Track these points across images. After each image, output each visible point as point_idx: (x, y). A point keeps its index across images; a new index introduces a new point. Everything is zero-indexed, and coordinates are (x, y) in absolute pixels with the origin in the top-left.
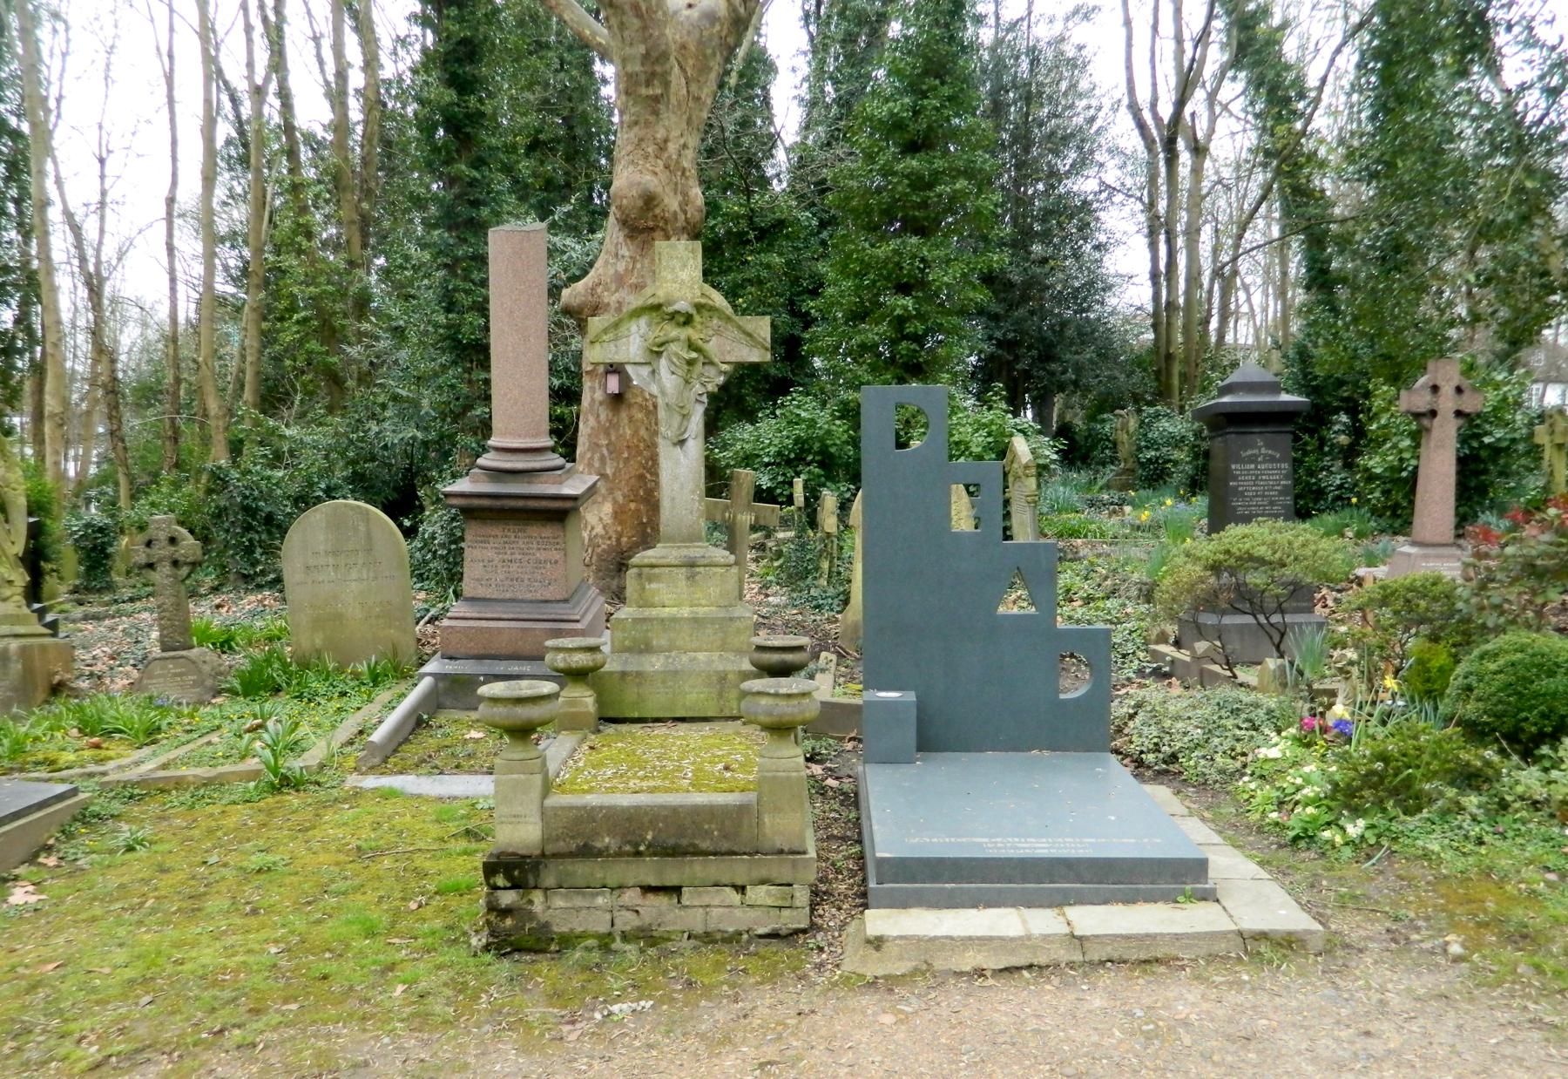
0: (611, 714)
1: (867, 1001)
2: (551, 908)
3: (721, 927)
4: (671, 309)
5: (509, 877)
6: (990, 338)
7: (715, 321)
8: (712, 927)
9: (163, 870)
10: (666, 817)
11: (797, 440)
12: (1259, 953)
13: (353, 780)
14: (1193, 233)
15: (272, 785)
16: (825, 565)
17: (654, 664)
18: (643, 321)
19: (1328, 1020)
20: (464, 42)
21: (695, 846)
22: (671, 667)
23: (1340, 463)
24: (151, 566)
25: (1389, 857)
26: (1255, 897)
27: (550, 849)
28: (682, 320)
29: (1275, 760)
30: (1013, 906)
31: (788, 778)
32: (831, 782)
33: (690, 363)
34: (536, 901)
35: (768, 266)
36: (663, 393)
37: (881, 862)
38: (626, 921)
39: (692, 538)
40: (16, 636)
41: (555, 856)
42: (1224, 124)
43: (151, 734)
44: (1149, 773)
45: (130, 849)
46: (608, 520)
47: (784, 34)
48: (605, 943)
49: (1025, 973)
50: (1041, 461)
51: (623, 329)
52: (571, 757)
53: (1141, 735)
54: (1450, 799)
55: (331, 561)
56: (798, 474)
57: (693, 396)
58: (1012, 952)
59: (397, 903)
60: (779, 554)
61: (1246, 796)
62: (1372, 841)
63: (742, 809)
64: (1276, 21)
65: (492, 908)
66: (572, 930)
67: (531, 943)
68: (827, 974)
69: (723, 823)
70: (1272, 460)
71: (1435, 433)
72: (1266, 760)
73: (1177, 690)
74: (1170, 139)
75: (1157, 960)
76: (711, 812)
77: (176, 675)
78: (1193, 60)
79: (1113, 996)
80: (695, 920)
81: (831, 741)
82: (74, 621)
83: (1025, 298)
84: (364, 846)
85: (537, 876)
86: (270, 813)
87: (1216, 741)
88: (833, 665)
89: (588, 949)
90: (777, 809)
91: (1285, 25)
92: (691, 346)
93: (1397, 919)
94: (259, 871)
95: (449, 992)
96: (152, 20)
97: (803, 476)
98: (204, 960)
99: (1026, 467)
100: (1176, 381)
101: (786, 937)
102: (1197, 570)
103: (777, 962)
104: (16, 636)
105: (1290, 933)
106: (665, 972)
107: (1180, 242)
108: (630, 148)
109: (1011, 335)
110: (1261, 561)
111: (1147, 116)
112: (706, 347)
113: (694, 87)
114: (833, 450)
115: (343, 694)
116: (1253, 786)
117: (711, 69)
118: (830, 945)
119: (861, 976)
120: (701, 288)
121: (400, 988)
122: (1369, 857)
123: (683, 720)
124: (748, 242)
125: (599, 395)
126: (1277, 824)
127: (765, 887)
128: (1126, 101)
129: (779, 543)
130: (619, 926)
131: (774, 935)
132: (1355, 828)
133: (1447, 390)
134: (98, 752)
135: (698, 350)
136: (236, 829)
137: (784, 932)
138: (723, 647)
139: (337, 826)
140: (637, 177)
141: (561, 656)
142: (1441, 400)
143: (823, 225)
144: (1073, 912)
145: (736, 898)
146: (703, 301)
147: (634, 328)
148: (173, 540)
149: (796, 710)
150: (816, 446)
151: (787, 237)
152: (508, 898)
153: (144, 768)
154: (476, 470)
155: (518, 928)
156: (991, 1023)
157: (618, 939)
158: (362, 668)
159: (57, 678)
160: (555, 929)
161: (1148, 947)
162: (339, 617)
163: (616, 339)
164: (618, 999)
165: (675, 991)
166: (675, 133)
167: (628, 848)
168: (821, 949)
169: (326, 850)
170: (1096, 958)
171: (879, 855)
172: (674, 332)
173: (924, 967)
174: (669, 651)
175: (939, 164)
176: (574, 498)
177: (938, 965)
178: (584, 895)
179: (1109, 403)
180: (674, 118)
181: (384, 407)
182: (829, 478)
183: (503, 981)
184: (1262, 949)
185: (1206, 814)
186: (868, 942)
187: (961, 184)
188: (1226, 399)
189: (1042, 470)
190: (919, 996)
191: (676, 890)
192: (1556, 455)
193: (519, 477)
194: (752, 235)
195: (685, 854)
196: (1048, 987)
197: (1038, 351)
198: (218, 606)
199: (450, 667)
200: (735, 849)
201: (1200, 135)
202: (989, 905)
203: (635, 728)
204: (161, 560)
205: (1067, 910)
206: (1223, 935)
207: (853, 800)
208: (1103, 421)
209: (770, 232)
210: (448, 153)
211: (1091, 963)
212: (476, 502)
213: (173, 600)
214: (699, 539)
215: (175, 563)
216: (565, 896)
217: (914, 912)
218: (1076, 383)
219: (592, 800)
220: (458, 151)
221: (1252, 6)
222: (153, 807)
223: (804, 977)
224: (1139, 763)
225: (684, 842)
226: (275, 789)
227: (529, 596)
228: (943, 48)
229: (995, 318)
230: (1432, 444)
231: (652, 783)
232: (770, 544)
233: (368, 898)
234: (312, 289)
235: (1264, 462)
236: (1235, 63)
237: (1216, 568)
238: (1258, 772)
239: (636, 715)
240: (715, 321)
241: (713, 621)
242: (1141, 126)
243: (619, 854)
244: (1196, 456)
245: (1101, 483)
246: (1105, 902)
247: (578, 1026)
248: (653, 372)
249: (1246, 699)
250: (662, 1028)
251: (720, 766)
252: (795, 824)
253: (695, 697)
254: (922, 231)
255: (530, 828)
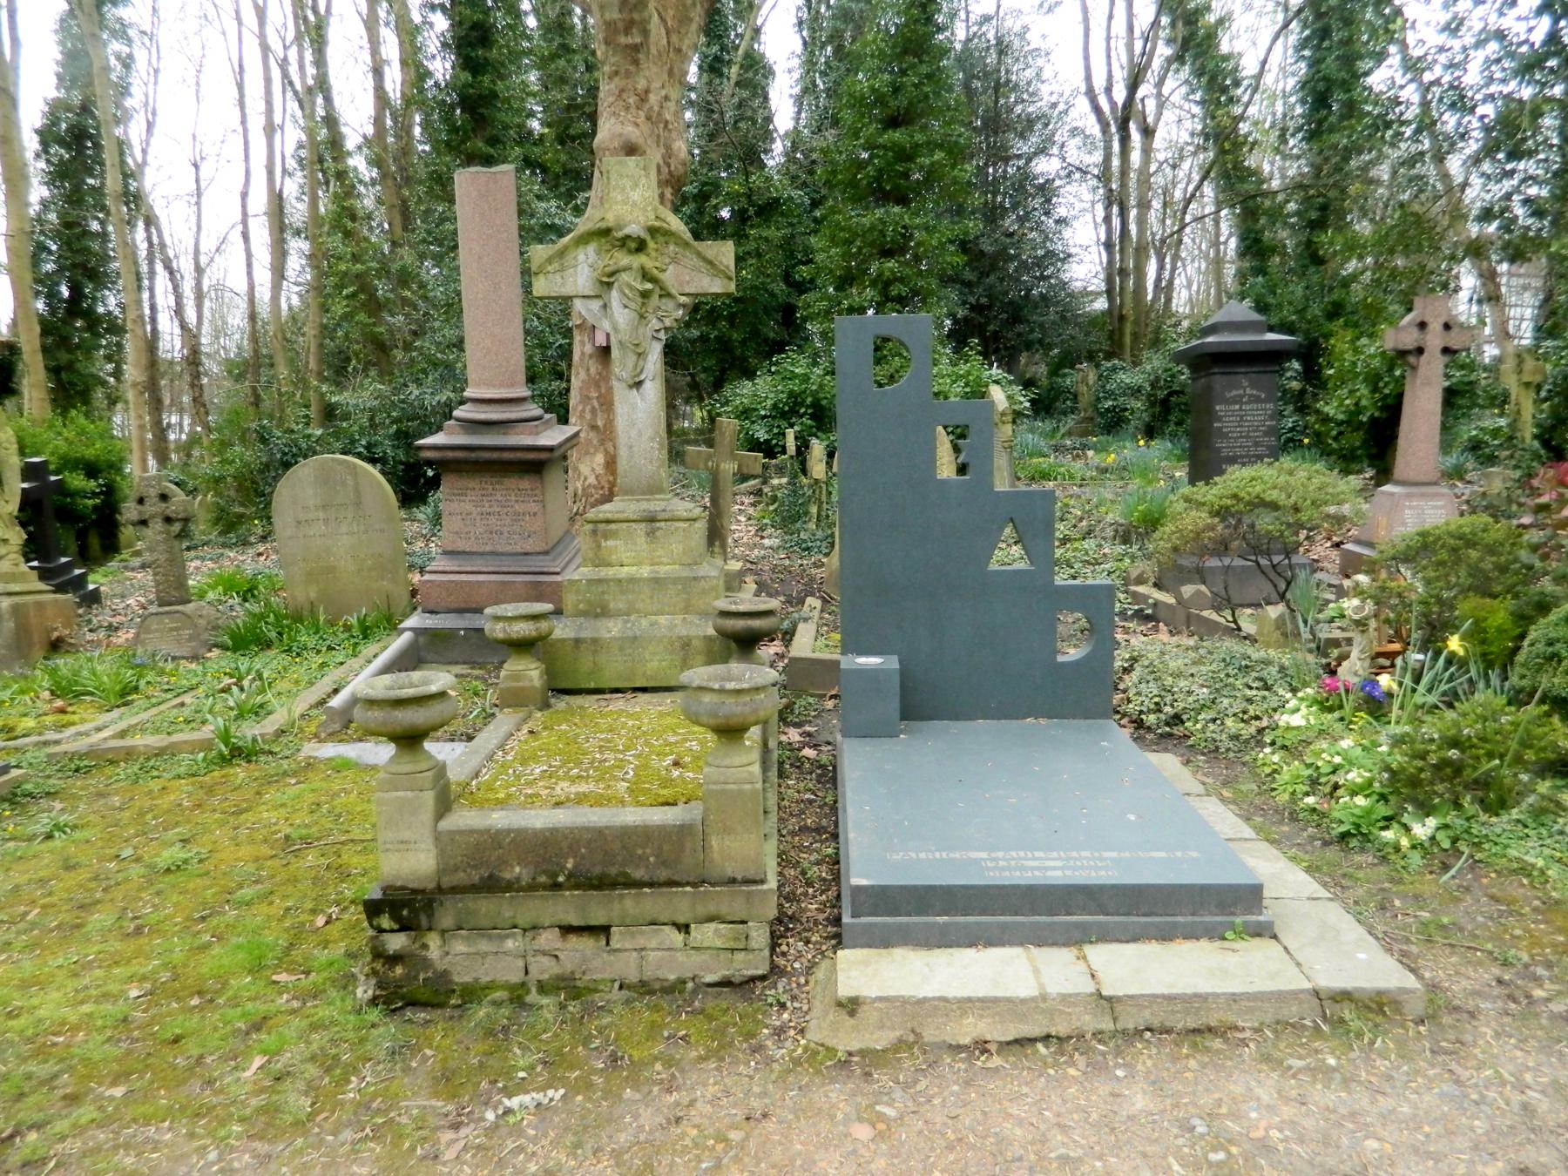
0: (564, 685)
1: (837, 1095)
2: (449, 953)
3: (661, 974)
4: (620, 234)
5: (395, 917)
6: (964, 303)
7: (672, 247)
8: (648, 975)
9: (69, 868)
10: (590, 841)
11: (791, 394)
12: (1342, 1021)
13: (312, 749)
14: (1144, 205)
15: (222, 756)
16: (814, 510)
17: (611, 629)
18: (591, 248)
19: (1462, 1143)
20: (475, 26)
21: (625, 874)
22: (630, 634)
23: (1291, 407)
24: (144, 523)
25: (1472, 868)
26: (1328, 942)
27: (447, 882)
28: (633, 245)
29: (1298, 728)
30: (1021, 944)
31: (740, 792)
32: (809, 752)
33: (645, 295)
34: (431, 944)
35: (767, 240)
36: (616, 329)
37: (858, 890)
38: (543, 968)
39: (652, 490)
40: (10, 594)
41: (455, 890)
42: (1169, 115)
43: (125, 694)
44: (1150, 736)
45: (49, 837)
46: (600, 470)
47: (780, 38)
48: (517, 996)
49: (1040, 1046)
50: (1016, 407)
51: (569, 258)
52: (501, 747)
53: (1139, 692)
54: (1543, 797)
55: (321, 515)
56: (791, 426)
57: (649, 334)
58: (1023, 1018)
59: (304, 917)
60: (774, 499)
61: (1268, 770)
62: (1446, 844)
63: (684, 830)
64: (1212, 18)
65: (378, 954)
66: (476, 980)
67: (424, 994)
68: (788, 1044)
69: (660, 848)
70: (1257, 400)
71: (1422, 370)
72: (1289, 728)
73: (1163, 636)
74: (1125, 120)
75: (1210, 1029)
76: (645, 834)
77: (171, 629)
78: (1143, 54)
79: (1157, 1086)
80: (627, 966)
81: (811, 700)
82: (133, 569)
83: (993, 267)
84: (294, 835)
85: (430, 916)
86: (210, 791)
87: (1226, 701)
88: (816, 614)
89: (497, 1004)
90: (727, 831)
91: (1221, 22)
92: (646, 276)
93: (1506, 964)
94: (168, 870)
95: (312, 1071)
96: (224, 33)
97: (797, 428)
98: (42, 1013)
99: (1003, 414)
100: (1128, 339)
101: (741, 984)
102: (1202, 518)
103: (727, 1025)
104: (10, 594)
105: (1380, 993)
106: (586, 1041)
107: (1133, 213)
108: (611, 99)
109: (984, 300)
110: (1274, 506)
111: (1106, 107)
112: (661, 276)
113: (674, 38)
114: (824, 402)
115: (330, 648)
116: (1276, 758)
117: (691, 20)
118: (794, 998)
119: (831, 1051)
120: (655, 209)
121: (258, 1061)
122: (1446, 867)
123: (644, 690)
124: (749, 217)
125: (588, 349)
126: (1314, 810)
127: (713, 926)
128: (1083, 89)
129: (773, 488)
130: (535, 973)
131: (726, 983)
132: (1423, 829)
133: (1435, 326)
134: (62, 716)
135: (654, 280)
136: (169, 811)
137: (737, 980)
138: (687, 610)
139: (280, 809)
140: (618, 129)
141: (501, 625)
142: (1429, 337)
143: (815, 204)
144: (1102, 955)
145: (678, 938)
146: (657, 224)
147: (581, 257)
148: (164, 497)
149: (747, 709)
150: (809, 400)
151: (782, 214)
152: (396, 942)
153: (96, 738)
154: (452, 422)
155: (411, 977)
156: (1001, 1140)
157: (534, 990)
158: (353, 621)
159: (55, 634)
160: (456, 979)
161: (1198, 1010)
162: (332, 569)
163: (562, 270)
164: (521, 1087)
165: (594, 1071)
166: (656, 85)
167: (543, 879)
168: (783, 1006)
169: (252, 841)
170: (1131, 1026)
171: (857, 881)
172: (624, 259)
173: (911, 1038)
174: (628, 615)
175: (919, 137)
176: (550, 449)
177: (930, 1035)
178: (490, 938)
179: (1069, 360)
180: (654, 69)
181: (424, 371)
182: (819, 429)
183: (382, 1055)
184: (1347, 1015)
185: (1226, 793)
186: (840, 1004)
187: (939, 155)
188: (1210, 339)
189: (1017, 415)
190: (906, 1086)
191: (603, 930)
192: (1523, 392)
193: (495, 428)
194: (751, 211)
195: (614, 885)
196: (1072, 1071)
197: (1004, 314)
198: (260, 554)
199: (430, 622)
200: (676, 878)
201: (1150, 120)
202: (990, 943)
203: (588, 701)
204: (153, 517)
205: (1089, 950)
206: (1295, 994)
207: (829, 776)
208: (1065, 375)
209: (769, 209)
210: (465, 132)
211: (1124, 1032)
212: (450, 454)
213: (167, 556)
214: (661, 491)
215: (168, 520)
216: (468, 938)
217: (898, 952)
218: (1040, 342)
219: (499, 819)
220: (474, 130)
221: (1193, 5)
222: (95, 781)
223: (758, 1049)
224: (1139, 724)
225: (613, 871)
226: (225, 761)
227: (508, 549)
228: (921, 29)
229: (969, 284)
230: (1418, 382)
231: (583, 788)
232: (766, 489)
233: (272, 910)
234: (358, 266)
235: (1249, 402)
236: (1179, 58)
237: (1221, 513)
238: (1279, 742)
239: (593, 685)
240: (672, 247)
241: (675, 581)
242: (1097, 109)
243: (533, 887)
244: (1152, 404)
245: (1063, 431)
246: (1135, 939)
247: (463, 1132)
248: (605, 306)
249: (1255, 656)
250: (569, 1139)
251: (669, 761)
252: (753, 848)
253: (654, 665)
254: (903, 201)
255: (422, 856)
